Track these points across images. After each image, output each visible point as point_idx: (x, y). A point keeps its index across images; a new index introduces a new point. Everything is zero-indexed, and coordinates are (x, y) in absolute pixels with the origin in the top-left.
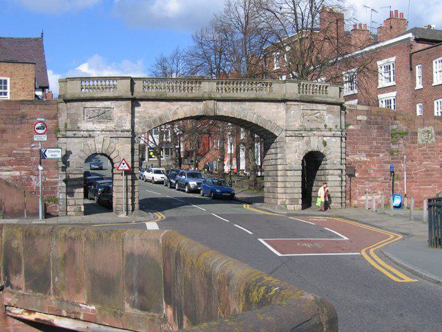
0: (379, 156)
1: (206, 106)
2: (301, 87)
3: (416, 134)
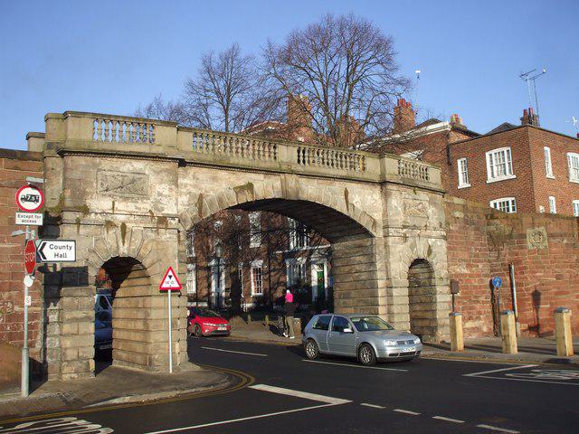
0: (478, 266)
1: (284, 183)
2: (301, 154)
3: (524, 236)
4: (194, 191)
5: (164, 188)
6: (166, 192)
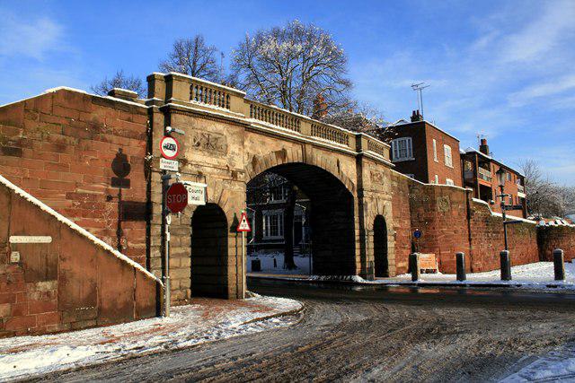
4: (251, 152)
5: (234, 148)
6: (237, 151)
